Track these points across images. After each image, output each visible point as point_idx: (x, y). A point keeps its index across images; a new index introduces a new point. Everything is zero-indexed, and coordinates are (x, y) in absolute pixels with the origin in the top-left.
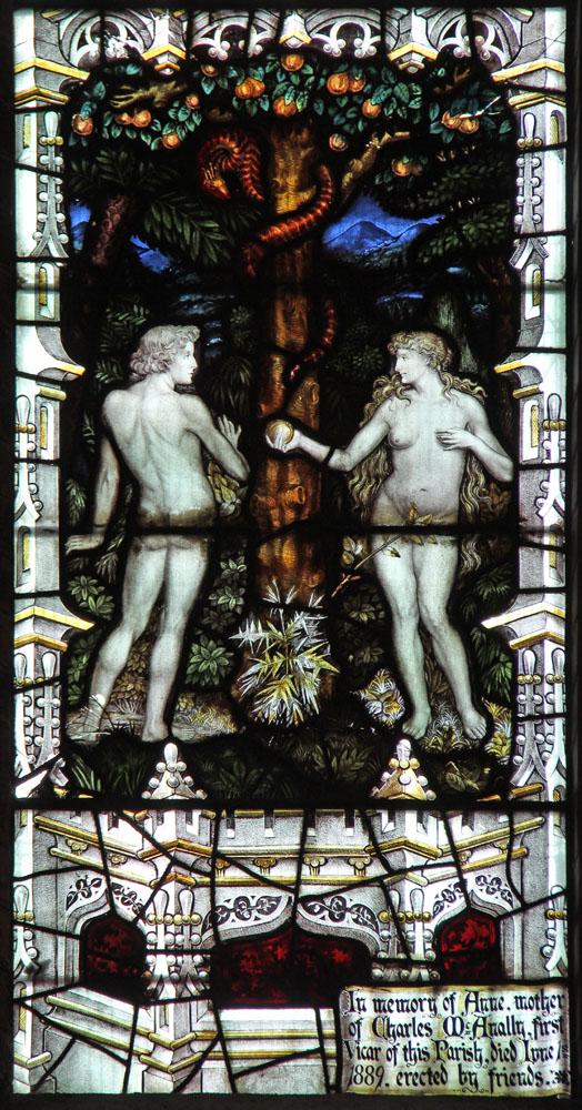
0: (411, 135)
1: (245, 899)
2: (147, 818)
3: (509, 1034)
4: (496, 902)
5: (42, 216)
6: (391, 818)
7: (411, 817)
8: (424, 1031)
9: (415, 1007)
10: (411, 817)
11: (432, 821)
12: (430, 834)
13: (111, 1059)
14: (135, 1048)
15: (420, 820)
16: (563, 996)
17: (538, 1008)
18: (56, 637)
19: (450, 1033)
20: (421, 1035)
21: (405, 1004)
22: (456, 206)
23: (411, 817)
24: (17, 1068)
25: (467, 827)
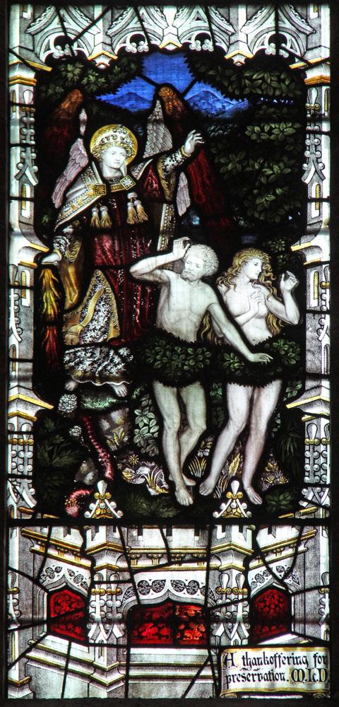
0: (52, 70)
1: (75, 581)
2: (88, 529)
3: (270, 680)
4: (69, 580)
5: (24, 154)
6: (224, 530)
7: (235, 529)
8: (241, 679)
9: (284, 659)
10: (235, 529)
11: (74, 531)
12: (240, 538)
13: (66, 685)
14: (63, 673)
15: (241, 530)
16: (326, 657)
17: (289, 664)
18: (31, 413)
19: (296, 680)
20: (239, 681)
21: (299, 660)
22: (285, 101)
23: (235, 529)
24: (191, 695)
25: (270, 535)
